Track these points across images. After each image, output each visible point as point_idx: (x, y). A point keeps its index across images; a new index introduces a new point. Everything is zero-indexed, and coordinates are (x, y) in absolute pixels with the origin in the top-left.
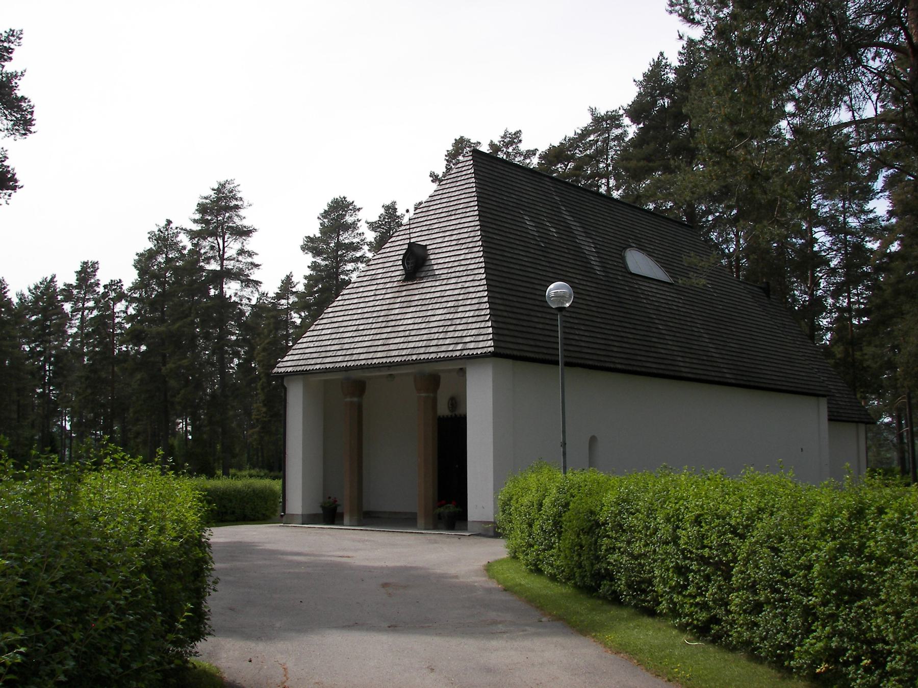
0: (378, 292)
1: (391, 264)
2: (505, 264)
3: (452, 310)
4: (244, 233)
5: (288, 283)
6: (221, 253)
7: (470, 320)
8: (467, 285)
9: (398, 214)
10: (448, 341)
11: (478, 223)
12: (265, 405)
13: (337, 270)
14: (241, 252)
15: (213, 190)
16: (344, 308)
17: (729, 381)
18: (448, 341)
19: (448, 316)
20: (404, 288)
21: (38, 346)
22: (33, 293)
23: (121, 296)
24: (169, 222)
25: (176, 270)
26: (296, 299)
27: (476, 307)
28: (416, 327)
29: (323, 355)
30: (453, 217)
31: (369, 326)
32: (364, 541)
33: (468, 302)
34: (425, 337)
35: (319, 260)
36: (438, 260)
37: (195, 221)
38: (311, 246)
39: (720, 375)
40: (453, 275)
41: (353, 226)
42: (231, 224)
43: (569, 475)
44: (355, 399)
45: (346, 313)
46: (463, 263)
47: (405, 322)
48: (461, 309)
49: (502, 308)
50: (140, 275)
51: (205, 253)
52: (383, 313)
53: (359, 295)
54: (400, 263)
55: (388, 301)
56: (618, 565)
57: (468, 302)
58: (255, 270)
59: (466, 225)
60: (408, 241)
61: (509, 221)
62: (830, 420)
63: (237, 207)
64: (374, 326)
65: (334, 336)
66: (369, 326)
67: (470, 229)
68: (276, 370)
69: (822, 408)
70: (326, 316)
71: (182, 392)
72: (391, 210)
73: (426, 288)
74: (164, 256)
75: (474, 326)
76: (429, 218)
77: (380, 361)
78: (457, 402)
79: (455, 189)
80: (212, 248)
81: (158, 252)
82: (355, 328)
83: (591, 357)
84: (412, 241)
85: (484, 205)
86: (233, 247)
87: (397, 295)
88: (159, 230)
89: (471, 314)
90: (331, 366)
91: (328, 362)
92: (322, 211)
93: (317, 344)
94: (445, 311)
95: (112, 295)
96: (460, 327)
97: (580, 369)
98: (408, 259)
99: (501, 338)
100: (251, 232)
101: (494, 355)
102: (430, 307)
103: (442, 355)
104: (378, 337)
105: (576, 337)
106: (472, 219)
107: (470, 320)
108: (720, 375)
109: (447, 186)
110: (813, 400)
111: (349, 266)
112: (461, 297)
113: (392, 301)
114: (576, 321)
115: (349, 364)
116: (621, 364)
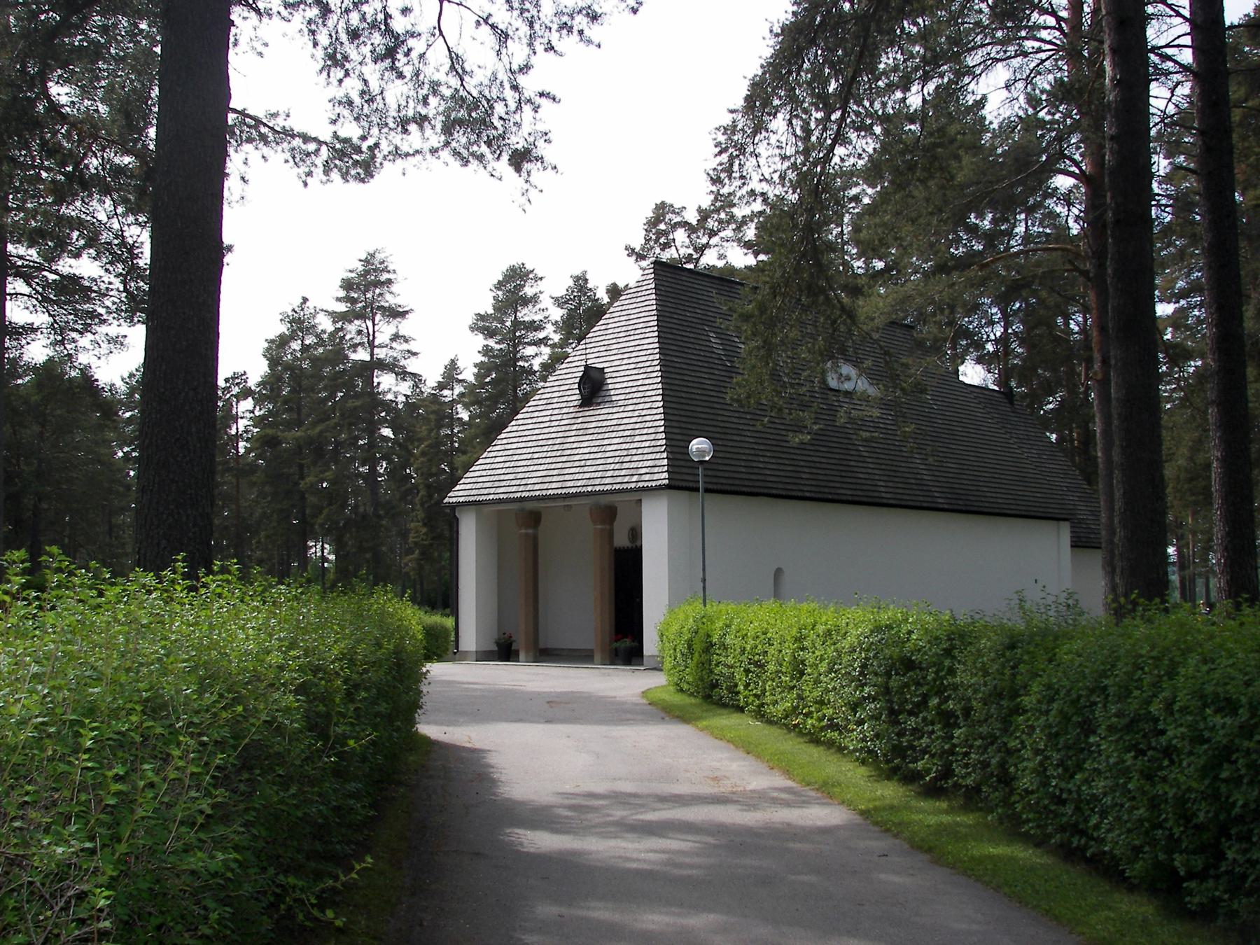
0: (553, 418)
1: (567, 387)
2: (685, 389)
3: (628, 439)
4: (396, 313)
5: (451, 370)
6: (371, 338)
7: (646, 451)
8: (644, 413)
9: (589, 286)
10: (623, 473)
11: (657, 345)
12: (425, 525)
13: (515, 355)
14: (396, 337)
15: (360, 260)
16: (518, 434)
17: (941, 506)
18: (623, 473)
19: (624, 446)
20: (581, 414)
21: (133, 450)
22: (127, 383)
23: (246, 393)
24: (305, 300)
25: (315, 361)
26: (462, 389)
27: (652, 437)
28: (592, 456)
29: (497, 484)
30: (632, 338)
31: (544, 455)
32: (538, 674)
33: (645, 431)
34: (600, 468)
35: (491, 343)
36: (615, 384)
37: (338, 299)
38: (483, 325)
39: (929, 499)
40: (630, 402)
41: (534, 300)
42: (382, 304)
43: (708, 606)
44: (530, 531)
45: (521, 439)
46: (641, 388)
47: (581, 451)
48: (637, 438)
49: (679, 437)
50: (270, 366)
51: (352, 339)
52: (558, 441)
53: (534, 420)
54: (576, 386)
55: (563, 428)
56: (721, 674)
57: (645, 431)
58: (413, 359)
59: (645, 347)
60: (583, 363)
61: (692, 340)
62: (1072, 546)
63: (389, 282)
64: (549, 454)
65: (507, 465)
66: (544, 455)
67: (649, 352)
68: (446, 500)
69: (1065, 533)
70: (499, 442)
71: (326, 511)
72: (581, 282)
73: (600, 415)
74: (299, 342)
75: (650, 457)
76: (608, 337)
77: (556, 492)
78: (635, 533)
79: (635, 306)
80: (359, 332)
81: (292, 337)
82: (529, 456)
83: (775, 486)
84: (589, 362)
85: (664, 324)
86: (384, 331)
87: (573, 421)
88: (294, 310)
89: (647, 444)
90: (505, 496)
91: (502, 493)
92: (496, 282)
93: (490, 472)
94: (622, 440)
95: (236, 390)
96: (635, 458)
97: (766, 499)
98: (584, 384)
99: (677, 470)
100: (407, 312)
101: (668, 487)
102: (606, 436)
103: (617, 487)
104: (553, 466)
105: (761, 465)
106: (652, 342)
107: (646, 451)
108: (929, 499)
109: (627, 302)
110: (1052, 524)
111: (530, 351)
112: (637, 426)
113: (568, 428)
114: (762, 447)
115: (523, 494)
116: (811, 492)
